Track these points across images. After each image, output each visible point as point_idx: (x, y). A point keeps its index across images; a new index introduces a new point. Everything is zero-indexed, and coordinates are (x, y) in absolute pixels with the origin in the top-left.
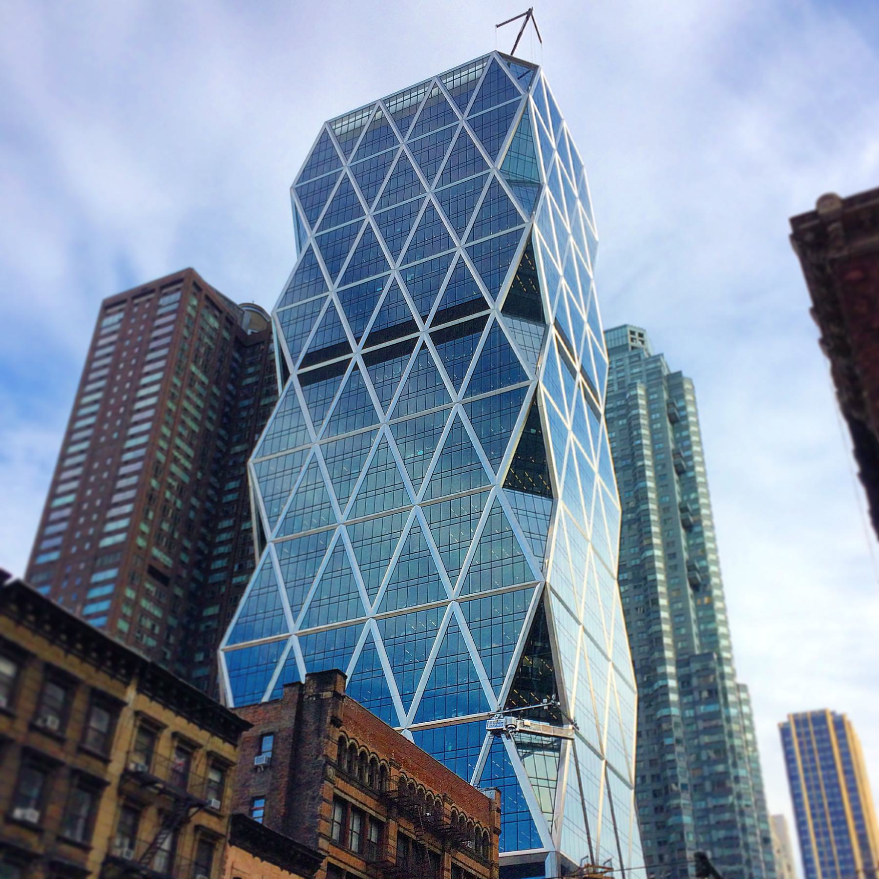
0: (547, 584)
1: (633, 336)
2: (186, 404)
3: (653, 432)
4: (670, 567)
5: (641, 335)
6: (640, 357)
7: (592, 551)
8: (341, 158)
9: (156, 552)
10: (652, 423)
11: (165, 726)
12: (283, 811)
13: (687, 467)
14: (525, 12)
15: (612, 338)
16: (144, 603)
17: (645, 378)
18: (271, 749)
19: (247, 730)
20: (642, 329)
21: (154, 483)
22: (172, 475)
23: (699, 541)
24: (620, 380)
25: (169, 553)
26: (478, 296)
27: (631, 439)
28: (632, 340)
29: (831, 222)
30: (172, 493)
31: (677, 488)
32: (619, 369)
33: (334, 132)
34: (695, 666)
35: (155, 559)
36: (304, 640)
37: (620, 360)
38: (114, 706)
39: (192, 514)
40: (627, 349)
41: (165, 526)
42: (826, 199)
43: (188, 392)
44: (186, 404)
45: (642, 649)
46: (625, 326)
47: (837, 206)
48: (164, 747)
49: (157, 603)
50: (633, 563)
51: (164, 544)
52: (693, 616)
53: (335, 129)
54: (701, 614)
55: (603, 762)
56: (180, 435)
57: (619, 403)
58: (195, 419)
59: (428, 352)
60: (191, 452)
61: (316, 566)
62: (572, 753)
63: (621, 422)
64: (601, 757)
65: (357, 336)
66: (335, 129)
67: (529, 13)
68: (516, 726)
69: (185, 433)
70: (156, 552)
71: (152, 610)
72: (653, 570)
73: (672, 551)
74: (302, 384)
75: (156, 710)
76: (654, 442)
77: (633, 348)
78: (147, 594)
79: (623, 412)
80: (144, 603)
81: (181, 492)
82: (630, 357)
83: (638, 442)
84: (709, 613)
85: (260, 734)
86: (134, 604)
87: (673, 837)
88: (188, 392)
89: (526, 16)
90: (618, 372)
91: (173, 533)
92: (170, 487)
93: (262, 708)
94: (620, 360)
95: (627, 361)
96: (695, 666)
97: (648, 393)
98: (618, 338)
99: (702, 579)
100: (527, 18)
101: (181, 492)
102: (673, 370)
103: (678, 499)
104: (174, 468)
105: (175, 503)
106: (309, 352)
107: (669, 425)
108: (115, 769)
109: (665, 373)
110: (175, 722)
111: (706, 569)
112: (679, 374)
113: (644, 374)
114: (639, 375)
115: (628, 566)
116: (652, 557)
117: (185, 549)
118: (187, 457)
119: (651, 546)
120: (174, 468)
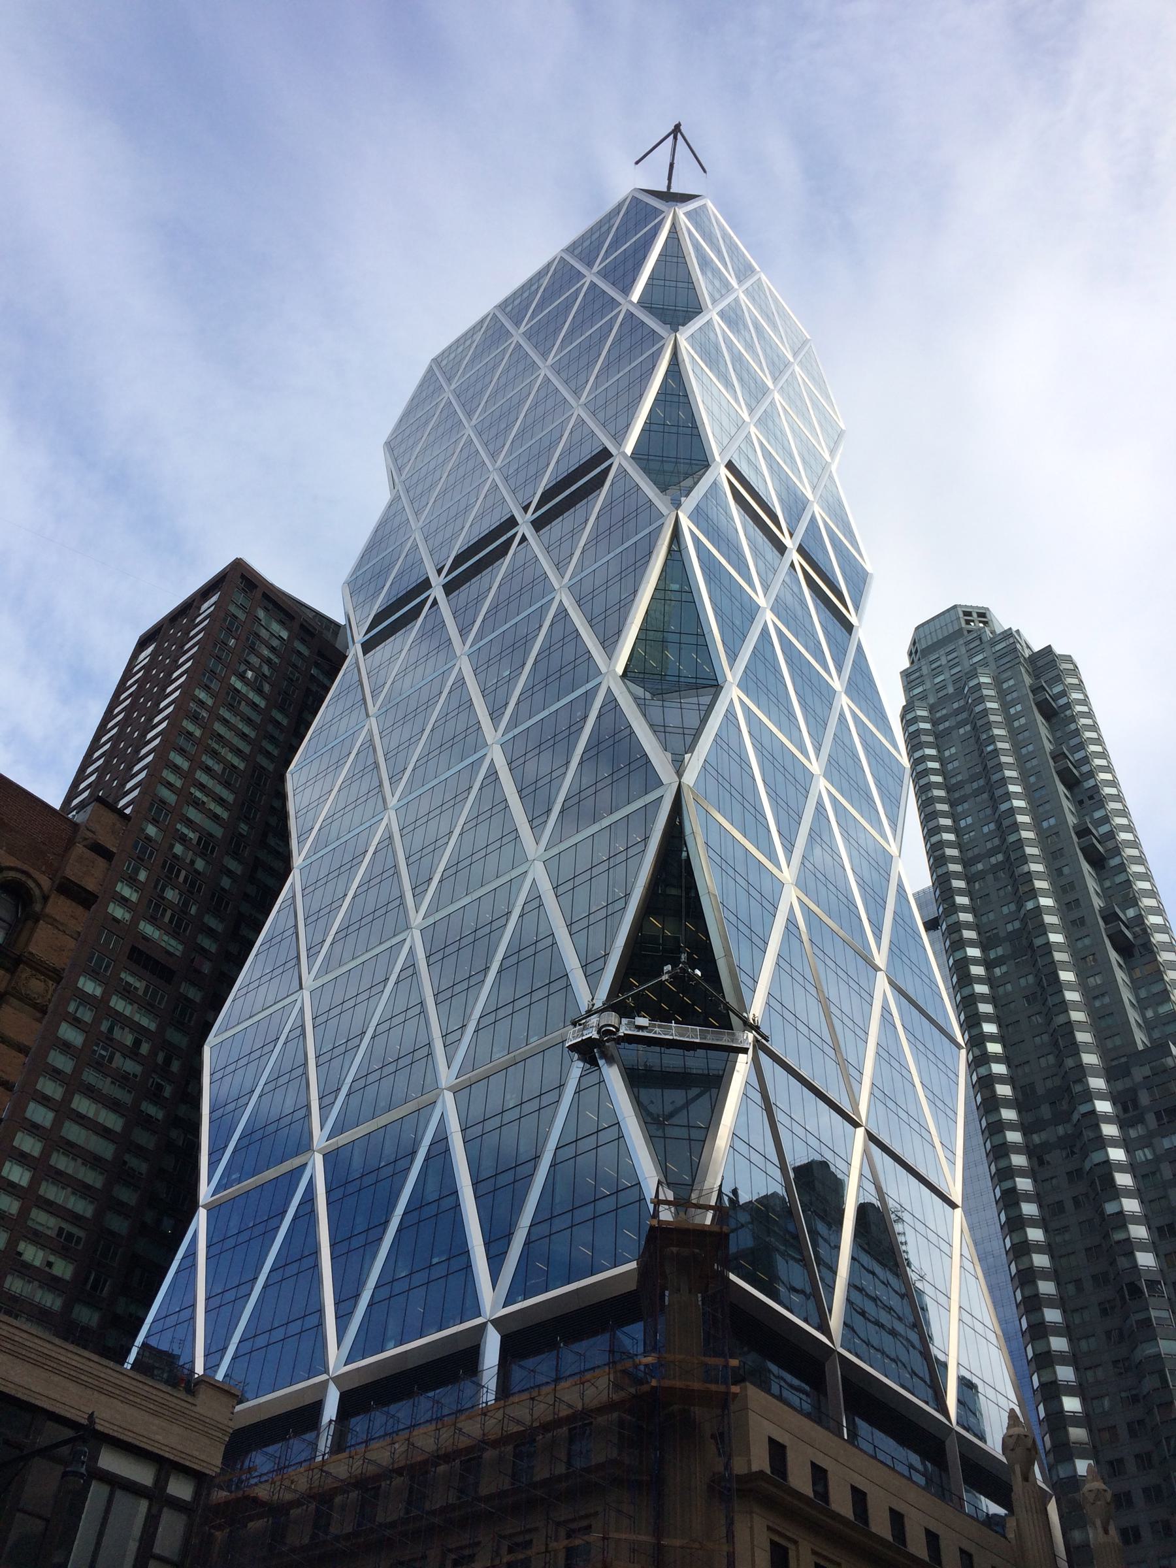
0: (685, 790)
2: (219, 728)
3: (1013, 734)
4: (1073, 922)
6: (980, 639)
9: (147, 929)
10: (1009, 720)
13: (1081, 775)
14: (670, 130)
16: (118, 1004)
17: (993, 665)
20: (983, 608)
21: (151, 830)
22: (189, 823)
23: (1120, 879)
24: (954, 678)
25: (175, 934)
27: (980, 745)
28: (968, 622)
30: (187, 848)
31: (1066, 804)
32: (952, 663)
34: (1139, 1073)
35: (146, 939)
37: (953, 651)
39: (226, 882)
40: (963, 635)
41: (171, 895)
43: (224, 713)
44: (219, 728)
45: (1042, 1060)
46: (955, 607)
49: (148, 1007)
50: (1010, 928)
51: (167, 919)
52: (1126, 995)
54: (1143, 994)
55: (860, 1132)
56: (208, 770)
57: (956, 706)
58: (238, 752)
60: (229, 796)
61: (349, 881)
62: (755, 1082)
63: (962, 731)
64: (856, 1125)
67: (677, 129)
68: (618, 1030)
69: (218, 768)
70: (147, 929)
71: (137, 1018)
72: (1043, 929)
73: (1071, 897)
76: (1016, 749)
77: (969, 632)
78: (127, 993)
79: (964, 715)
80: (118, 1004)
81: (206, 845)
82: (967, 643)
83: (990, 748)
84: (1156, 989)
86: (100, 1005)
87: (1150, 1383)
88: (224, 713)
89: (672, 136)
90: (951, 668)
91: (186, 904)
92: (183, 839)
94: (953, 651)
95: (963, 650)
96: (1139, 1073)
97: (998, 682)
99: (1135, 936)
100: (675, 138)
101: (205, 847)
102: (1037, 647)
103: (1071, 820)
104: (192, 813)
105: (193, 862)
107: (1039, 718)
109: (1027, 653)
111: (1139, 919)
112: (1048, 650)
113: (991, 660)
114: (984, 663)
115: (1002, 934)
116: (1038, 910)
117: (210, 933)
118: (221, 801)
119: (1033, 894)
120: (192, 813)
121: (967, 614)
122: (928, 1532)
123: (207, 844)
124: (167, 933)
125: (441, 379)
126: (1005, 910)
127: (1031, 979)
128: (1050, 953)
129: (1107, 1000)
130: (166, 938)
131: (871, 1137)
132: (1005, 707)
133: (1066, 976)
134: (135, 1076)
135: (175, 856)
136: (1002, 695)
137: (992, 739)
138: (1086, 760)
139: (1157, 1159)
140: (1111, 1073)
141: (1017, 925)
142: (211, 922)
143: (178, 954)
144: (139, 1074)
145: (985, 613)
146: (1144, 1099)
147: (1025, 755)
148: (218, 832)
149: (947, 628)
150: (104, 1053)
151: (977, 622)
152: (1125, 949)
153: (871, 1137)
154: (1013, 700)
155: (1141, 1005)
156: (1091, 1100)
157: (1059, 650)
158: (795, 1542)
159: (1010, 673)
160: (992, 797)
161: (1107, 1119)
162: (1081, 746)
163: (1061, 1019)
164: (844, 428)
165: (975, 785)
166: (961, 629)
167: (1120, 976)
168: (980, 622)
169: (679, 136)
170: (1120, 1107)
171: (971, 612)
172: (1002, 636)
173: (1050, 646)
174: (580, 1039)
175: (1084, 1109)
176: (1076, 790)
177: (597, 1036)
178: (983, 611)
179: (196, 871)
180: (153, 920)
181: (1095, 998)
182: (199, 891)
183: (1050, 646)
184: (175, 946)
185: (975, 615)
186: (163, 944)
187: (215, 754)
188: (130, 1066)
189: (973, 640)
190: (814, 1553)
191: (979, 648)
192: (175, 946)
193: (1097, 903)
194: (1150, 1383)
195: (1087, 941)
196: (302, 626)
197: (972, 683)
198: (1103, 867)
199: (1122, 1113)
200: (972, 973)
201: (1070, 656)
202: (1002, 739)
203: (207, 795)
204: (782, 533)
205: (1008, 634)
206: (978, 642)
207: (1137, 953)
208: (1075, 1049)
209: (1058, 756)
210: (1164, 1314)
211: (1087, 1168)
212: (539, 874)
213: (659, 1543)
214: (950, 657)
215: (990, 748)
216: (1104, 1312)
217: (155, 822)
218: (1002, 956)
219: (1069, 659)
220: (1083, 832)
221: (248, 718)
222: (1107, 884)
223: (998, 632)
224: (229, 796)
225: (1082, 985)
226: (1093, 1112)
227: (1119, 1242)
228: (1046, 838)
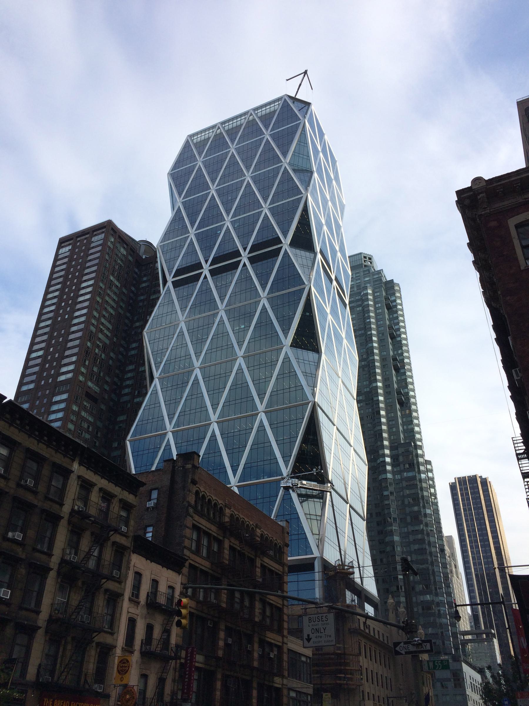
2: (107, 298)
5: (370, 259)
7: (342, 384)
9: (90, 384)
10: (376, 309)
16: (83, 414)
22: (99, 339)
23: (403, 377)
24: (358, 284)
25: (97, 385)
28: (365, 261)
34: (401, 450)
35: (89, 387)
38: (66, 473)
41: (95, 369)
42: (477, 180)
44: (107, 298)
46: (361, 253)
49: (91, 414)
50: (365, 390)
52: (400, 421)
59: (247, 268)
63: (358, 309)
67: (306, 73)
68: (298, 485)
70: (90, 384)
72: (377, 395)
75: (90, 476)
76: (377, 320)
77: (365, 266)
78: (85, 409)
79: (360, 303)
80: (83, 414)
82: (364, 271)
83: (368, 320)
92: (98, 346)
96: (401, 450)
97: (374, 292)
98: (355, 261)
104: (100, 336)
105: (101, 355)
107: (386, 311)
108: (66, 509)
109: (384, 280)
110: (102, 483)
116: (377, 387)
118: (108, 329)
120: (100, 336)
121: (365, 257)
122: (373, 628)
123: (105, 347)
124: (95, 385)
126: (365, 383)
127: (370, 410)
128: (379, 404)
129: (394, 422)
130: (94, 386)
131: (350, 506)
132: (375, 303)
133: (383, 413)
134: (89, 439)
135: (96, 354)
136: (375, 297)
137: (369, 317)
138: (399, 329)
139: (402, 480)
140: (391, 448)
141: (368, 390)
142: (107, 379)
143: (98, 392)
144: (89, 438)
145: (371, 258)
146: (401, 459)
148: (107, 342)
149: (357, 262)
150: (80, 432)
151: (368, 262)
152: (401, 404)
153: (350, 506)
154: (378, 301)
155: (403, 424)
156: (384, 457)
157: (395, 281)
158: (361, 641)
159: (378, 290)
160: (486, 604)
161: (388, 464)
162: (398, 323)
163: (378, 428)
164: (345, 204)
165: (360, 332)
166: (362, 264)
167: (399, 413)
168: (369, 261)
169: (306, 75)
170: (393, 460)
171: (366, 257)
172: (377, 272)
173: (393, 280)
174: (286, 485)
175: (381, 459)
176: (394, 340)
177: (291, 486)
178: (371, 257)
179: (102, 359)
180: (91, 380)
181: (390, 421)
182: (103, 367)
183: (393, 280)
184: (96, 389)
185: (368, 258)
186: (94, 389)
187: (106, 309)
188: (87, 436)
189: (366, 271)
190: (364, 642)
191: (368, 275)
192: (96, 389)
193: (396, 386)
194: (388, 549)
195: (390, 400)
196: (131, 249)
197: (365, 292)
198: (398, 372)
199: (393, 462)
200: (387, 469)
201: (399, 284)
202: (373, 317)
203: (104, 327)
205: (380, 272)
206: (368, 272)
207: (405, 406)
208: (382, 439)
209: (390, 327)
210: (397, 528)
211: (380, 479)
212: (183, 325)
213: (344, 647)
214: (357, 275)
215: (368, 320)
216: (378, 525)
217: (90, 341)
218: (362, 400)
219: (398, 285)
220: (395, 359)
221: (115, 293)
222: (399, 378)
223: (376, 270)
224: (110, 327)
225: (387, 417)
226: (385, 461)
227: (386, 504)
228: (383, 360)
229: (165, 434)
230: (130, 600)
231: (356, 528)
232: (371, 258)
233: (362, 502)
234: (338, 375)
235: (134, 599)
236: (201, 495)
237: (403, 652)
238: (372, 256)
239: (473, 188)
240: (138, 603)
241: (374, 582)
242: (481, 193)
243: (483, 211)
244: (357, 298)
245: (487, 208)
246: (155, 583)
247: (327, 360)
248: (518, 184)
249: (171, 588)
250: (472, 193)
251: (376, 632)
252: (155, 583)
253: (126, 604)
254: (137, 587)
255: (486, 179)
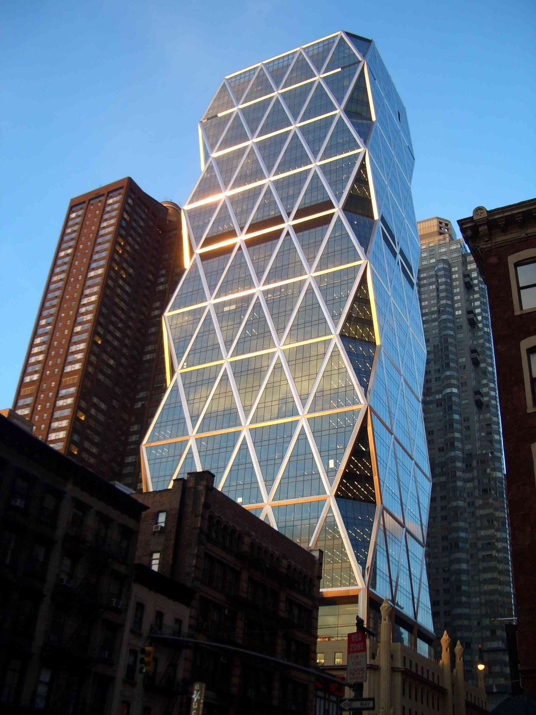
1: (441, 225)
5: (447, 225)
7: (403, 382)
8: (234, 101)
11: (92, 507)
12: (501, 568)
15: (427, 226)
18: (164, 521)
19: (145, 510)
26: (328, 199)
29: (481, 225)
33: (230, 85)
36: (199, 441)
38: (59, 495)
42: (479, 210)
47: (485, 215)
48: (91, 521)
53: (231, 82)
55: (405, 529)
59: (291, 238)
65: (241, 226)
66: (231, 82)
74: (202, 260)
75: (85, 497)
79: (434, 280)
85: (157, 511)
93: (159, 494)
98: (431, 227)
106: (208, 237)
108: (60, 533)
110: (98, 505)
117: (124, 355)
125: (218, 177)
127: (441, 413)
147: (461, 362)
168: (446, 228)
185: (444, 224)
198: (478, 366)
204: (382, 227)
229: (187, 441)
230: (132, 631)
231: (412, 556)
232: (448, 224)
233: (422, 525)
234: (399, 371)
235: (136, 632)
236: (215, 520)
237: (347, 708)
238: (450, 222)
239: (475, 219)
240: (141, 635)
241: (431, 616)
242: (484, 224)
243: (484, 245)
244: (431, 273)
245: (488, 241)
246: (159, 615)
247: (414, 333)
248: (520, 218)
249: (178, 621)
250: (474, 224)
251: (430, 673)
252: (159, 615)
253: (127, 635)
254: (138, 621)
255: (488, 209)
